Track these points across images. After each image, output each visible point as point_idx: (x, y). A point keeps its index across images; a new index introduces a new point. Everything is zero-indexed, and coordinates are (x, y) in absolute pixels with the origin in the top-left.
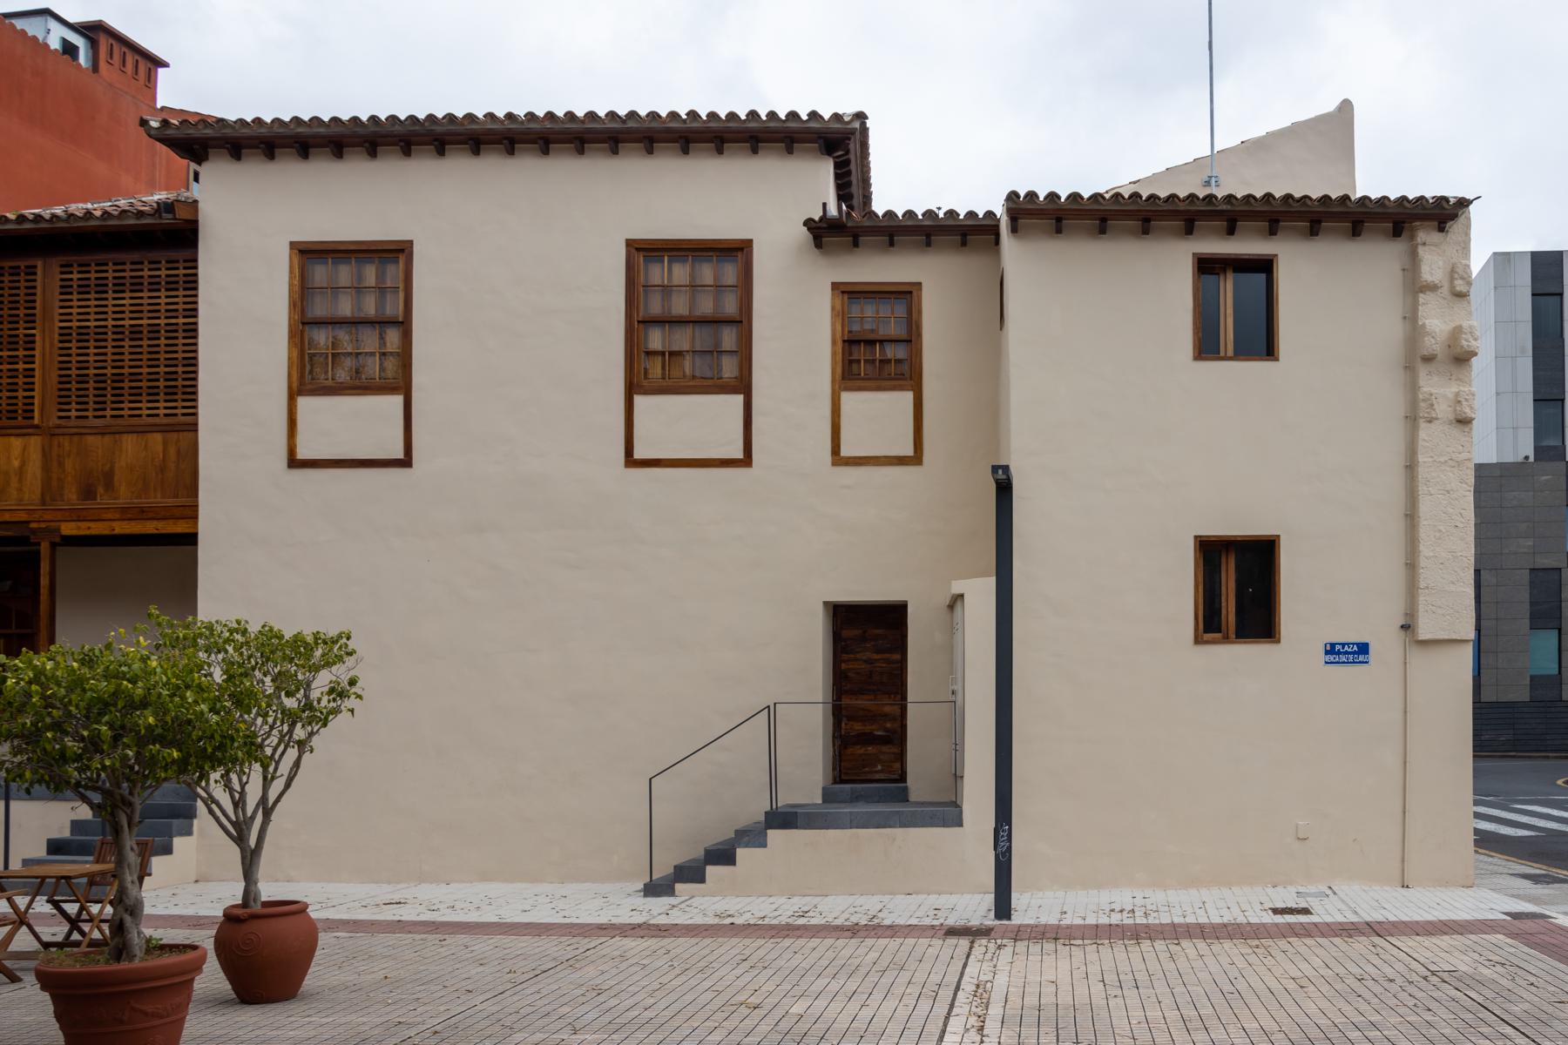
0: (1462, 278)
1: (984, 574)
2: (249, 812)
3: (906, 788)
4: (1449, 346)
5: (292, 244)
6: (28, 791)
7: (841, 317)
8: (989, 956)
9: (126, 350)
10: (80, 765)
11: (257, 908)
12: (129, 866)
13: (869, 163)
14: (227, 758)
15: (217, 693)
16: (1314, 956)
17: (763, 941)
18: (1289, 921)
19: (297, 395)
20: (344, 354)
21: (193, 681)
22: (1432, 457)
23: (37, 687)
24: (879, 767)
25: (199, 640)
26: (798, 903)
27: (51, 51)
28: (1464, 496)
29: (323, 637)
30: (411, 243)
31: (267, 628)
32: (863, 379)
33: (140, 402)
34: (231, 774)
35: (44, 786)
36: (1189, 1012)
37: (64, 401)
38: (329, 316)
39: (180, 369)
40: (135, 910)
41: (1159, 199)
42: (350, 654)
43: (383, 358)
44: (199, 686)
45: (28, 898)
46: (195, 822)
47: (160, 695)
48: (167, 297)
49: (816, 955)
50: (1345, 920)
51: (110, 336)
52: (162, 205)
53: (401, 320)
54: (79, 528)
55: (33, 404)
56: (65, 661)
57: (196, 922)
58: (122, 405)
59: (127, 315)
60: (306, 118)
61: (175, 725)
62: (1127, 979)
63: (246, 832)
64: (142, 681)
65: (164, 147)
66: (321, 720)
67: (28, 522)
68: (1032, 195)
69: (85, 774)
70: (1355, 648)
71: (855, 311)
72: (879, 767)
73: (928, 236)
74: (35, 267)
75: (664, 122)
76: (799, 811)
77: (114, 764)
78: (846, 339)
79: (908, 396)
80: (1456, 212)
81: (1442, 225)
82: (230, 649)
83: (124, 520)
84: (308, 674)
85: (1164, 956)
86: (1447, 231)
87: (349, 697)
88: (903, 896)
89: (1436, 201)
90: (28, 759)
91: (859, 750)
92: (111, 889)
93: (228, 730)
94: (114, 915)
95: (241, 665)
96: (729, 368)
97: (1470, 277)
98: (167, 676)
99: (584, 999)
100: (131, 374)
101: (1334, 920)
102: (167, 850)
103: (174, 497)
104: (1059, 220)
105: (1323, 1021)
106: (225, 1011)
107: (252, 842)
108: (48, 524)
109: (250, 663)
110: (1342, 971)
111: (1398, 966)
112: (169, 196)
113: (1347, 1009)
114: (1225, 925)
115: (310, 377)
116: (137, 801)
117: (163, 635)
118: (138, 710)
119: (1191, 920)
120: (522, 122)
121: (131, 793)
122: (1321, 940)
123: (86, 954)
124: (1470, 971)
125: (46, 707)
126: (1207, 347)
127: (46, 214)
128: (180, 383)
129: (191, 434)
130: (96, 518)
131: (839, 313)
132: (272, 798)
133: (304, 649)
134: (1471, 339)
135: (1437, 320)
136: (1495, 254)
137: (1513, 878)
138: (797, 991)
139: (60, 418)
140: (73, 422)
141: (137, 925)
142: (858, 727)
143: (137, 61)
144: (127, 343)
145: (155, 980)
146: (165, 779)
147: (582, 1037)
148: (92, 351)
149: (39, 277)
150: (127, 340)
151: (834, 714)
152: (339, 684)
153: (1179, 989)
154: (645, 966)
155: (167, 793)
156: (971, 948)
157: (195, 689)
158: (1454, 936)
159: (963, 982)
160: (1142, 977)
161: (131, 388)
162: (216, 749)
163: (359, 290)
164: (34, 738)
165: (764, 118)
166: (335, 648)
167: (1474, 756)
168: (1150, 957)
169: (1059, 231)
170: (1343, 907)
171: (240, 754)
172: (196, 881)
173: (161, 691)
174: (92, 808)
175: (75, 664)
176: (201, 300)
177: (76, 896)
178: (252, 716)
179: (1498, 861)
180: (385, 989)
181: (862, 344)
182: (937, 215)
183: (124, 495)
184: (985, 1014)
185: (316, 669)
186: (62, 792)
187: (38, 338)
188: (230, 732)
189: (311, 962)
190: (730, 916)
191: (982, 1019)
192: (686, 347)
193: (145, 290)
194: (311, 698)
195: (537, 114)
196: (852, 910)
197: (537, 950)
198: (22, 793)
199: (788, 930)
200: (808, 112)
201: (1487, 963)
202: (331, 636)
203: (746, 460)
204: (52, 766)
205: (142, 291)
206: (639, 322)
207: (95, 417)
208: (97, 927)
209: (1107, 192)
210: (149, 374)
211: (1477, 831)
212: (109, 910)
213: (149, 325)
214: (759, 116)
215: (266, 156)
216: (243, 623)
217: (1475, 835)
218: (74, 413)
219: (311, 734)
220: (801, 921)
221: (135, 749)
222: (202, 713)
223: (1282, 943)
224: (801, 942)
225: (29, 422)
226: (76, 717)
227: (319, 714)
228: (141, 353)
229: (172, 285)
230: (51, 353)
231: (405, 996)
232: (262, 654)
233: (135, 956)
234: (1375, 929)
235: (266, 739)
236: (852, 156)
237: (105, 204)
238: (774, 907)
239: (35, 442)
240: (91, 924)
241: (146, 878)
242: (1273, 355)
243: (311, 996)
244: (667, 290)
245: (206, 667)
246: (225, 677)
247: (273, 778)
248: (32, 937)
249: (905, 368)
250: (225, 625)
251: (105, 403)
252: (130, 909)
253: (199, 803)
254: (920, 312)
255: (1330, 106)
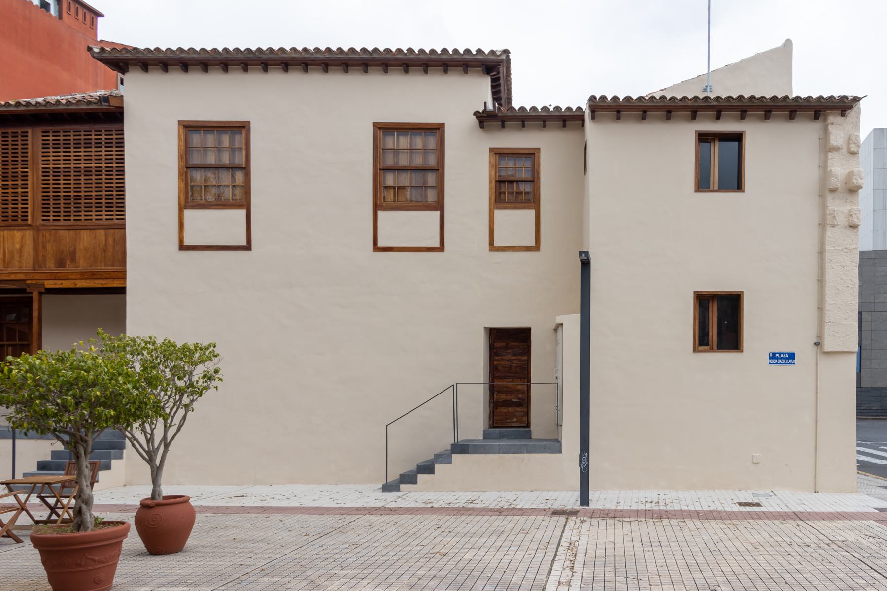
0: (855, 143)
1: (574, 312)
2: (156, 446)
3: (530, 431)
4: (846, 183)
5: (179, 122)
6: (26, 434)
7: (494, 168)
8: (576, 526)
9: (82, 181)
10: (56, 419)
11: (160, 500)
12: (85, 476)
13: (511, 79)
14: (143, 415)
15: (137, 378)
16: (763, 530)
17: (450, 517)
18: (748, 510)
19: (184, 209)
20: (212, 186)
21: (123, 371)
22: (834, 247)
23: (31, 375)
24: (515, 420)
25: (127, 348)
26: (469, 495)
27: (34, 6)
28: (853, 269)
29: (200, 346)
30: (249, 122)
31: (167, 341)
32: (507, 203)
33: (91, 211)
34: (145, 424)
35: (35, 431)
36: (691, 561)
37: (45, 211)
38: (202, 164)
39: (115, 193)
40: (88, 502)
41: (677, 99)
42: (215, 356)
43: (234, 188)
44: (127, 374)
45: (26, 495)
46: (125, 451)
47: (103, 379)
48: (106, 151)
49: (479, 525)
50: (781, 510)
51: (73, 173)
52: (102, 98)
53: (244, 167)
54: (56, 284)
55: (27, 212)
56: (47, 360)
57: (125, 508)
58: (80, 214)
59: (83, 161)
60: (186, 48)
61: (112, 396)
62: (655, 541)
63: (154, 457)
64: (93, 371)
65: (103, 64)
66: (198, 393)
67: (25, 280)
68: (603, 98)
69: (59, 424)
70: (787, 356)
71: (503, 164)
72: (515, 420)
73: (544, 121)
74: (27, 132)
75: (394, 55)
76: (470, 443)
77: (76, 419)
78: (497, 180)
79: (532, 212)
80: (851, 105)
81: (844, 112)
82: (145, 353)
83: (82, 279)
84: (191, 367)
85: (676, 528)
86: (847, 116)
87: (215, 380)
88: (528, 492)
89: (840, 99)
90: (25, 416)
91: (504, 410)
92: (74, 490)
93: (144, 399)
94: (76, 505)
95: (151, 362)
96: (431, 196)
97: (859, 143)
98: (108, 368)
99: (348, 550)
100: (85, 195)
101: (774, 510)
102: (108, 467)
103: (112, 266)
104: (619, 112)
105: (768, 568)
106: (141, 559)
107: (158, 462)
108: (37, 281)
109: (157, 361)
110: (779, 540)
111: (812, 537)
112: (106, 93)
113: (782, 561)
114: (711, 512)
115: (192, 198)
116: (90, 439)
117: (106, 345)
118: (90, 387)
119: (691, 508)
120: (312, 53)
121: (86, 435)
122: (767, 522)
123: (59, 527)
124: (854, 541)
125: (36, 386)
126: (703, 184)
127: (33, 102)
128: (114, 201)
129: (122, 231)
130: (65, 278)
131: (493, 166)
132: (169, 436)
133: (189, 352)
134: (859, 179)
135: (839, 168)
136: (875, 129)
137: (880, 488)
138: (468, 545)
139: (43, 220)
140: (51, 223)
141: (89, 510)
142: (503, 397)
143: (85, 13)
144: (83, 178)
145: (106, 540)
146: (107, 427)
147: (346, 572)
148: (62, 182)
149: (29, 138)
150: (83, 176)
151: (490, 390)
152: (208, 372)
153: (685, 548)
154: (382, 531)
155: (108, 435)
156: (566, 522)
157: (125, 376)
158: (845, 521)
159: (562, 541)
160: (664, 540)
161: (85, 203)
162: (136, 409)
163: (219, 149)
164: (30, 404)
165: (451, 53)
166: (206, 353)
167: (857, 418)
168: (668, 528)
169: (618, 118)
170: (779, 502)
171: (150, 412)
172: (125, 485)
173: (104, 377)
174: (63, 444)
175: (53, 362)
176: (126, 153)
177: (54, 494)
178: (158, 391)
179: (871, 479)
180: (235, 545)
181: (506, 183)
182: (549, 110)
183: (82, 264)
184: (574, 560)
185: (196, 364)
186: (45, 434)
187: (29, 174)
188: (145, 400)
189: (191, 530)
190: (431, 503)
191: (572, 562)
192: (407, 184)
193: (93, 147)
194: (193, 380)
195: (321, 49)
196: (499, 500)
197: (321, 522)
198: (23, 435)
199: (464, 511)
200: (476, 49)
201: (864, 537)
202: (204, 345)
203: (441, 248)
204: (39, 419)
205: (91, 147)
206: (380, 169)
207: (65, 220)
208: (67, 512)
209: (647, 96)
210: (96, 195)
211: (859, 461)
212: (73, 502)
213: (96, 167)
214: (448, 51)
215: (163, 70)
216: (153, 338)
217: (857, 463)
218: (51, 218)
219: (192, 401)
220: (471, 506)
221: (88, 410)
222: (128, 389)
223: (745, 523)
224: (471, 517)
225: (24, 222)
226: (54, 392)
227: (197, 390)
228: (91, 183)
229: (109, 144)
230: (37, 183)
231: (244, 550)
232: (164, 355)
233: (88, 528)
234: (798, 516)
235: (166, 404)
236: (501, 75)
237: (68, 97)
238: (456, 497)
239: (29, 234)
240: (63, 510)
241: (95, 484)
242: (741, 189)
243: (191, 550)
244: (396, 151)
245: (131, 363)
246: (142, 368)
247: (170, 426)
248: (28, 518)
249: (530, 196)
250: (143, 340)
251: (70, 212)
252: (85, 501)
253: (127, 441)
254: (539, 165)
255: (779, 43)
